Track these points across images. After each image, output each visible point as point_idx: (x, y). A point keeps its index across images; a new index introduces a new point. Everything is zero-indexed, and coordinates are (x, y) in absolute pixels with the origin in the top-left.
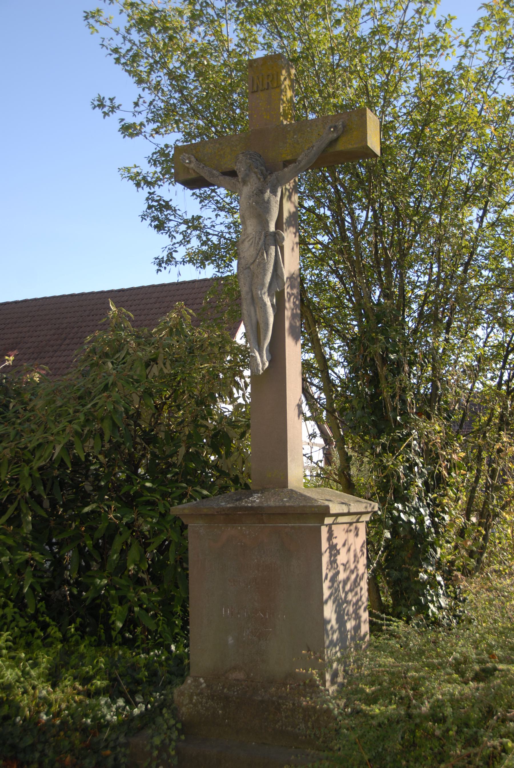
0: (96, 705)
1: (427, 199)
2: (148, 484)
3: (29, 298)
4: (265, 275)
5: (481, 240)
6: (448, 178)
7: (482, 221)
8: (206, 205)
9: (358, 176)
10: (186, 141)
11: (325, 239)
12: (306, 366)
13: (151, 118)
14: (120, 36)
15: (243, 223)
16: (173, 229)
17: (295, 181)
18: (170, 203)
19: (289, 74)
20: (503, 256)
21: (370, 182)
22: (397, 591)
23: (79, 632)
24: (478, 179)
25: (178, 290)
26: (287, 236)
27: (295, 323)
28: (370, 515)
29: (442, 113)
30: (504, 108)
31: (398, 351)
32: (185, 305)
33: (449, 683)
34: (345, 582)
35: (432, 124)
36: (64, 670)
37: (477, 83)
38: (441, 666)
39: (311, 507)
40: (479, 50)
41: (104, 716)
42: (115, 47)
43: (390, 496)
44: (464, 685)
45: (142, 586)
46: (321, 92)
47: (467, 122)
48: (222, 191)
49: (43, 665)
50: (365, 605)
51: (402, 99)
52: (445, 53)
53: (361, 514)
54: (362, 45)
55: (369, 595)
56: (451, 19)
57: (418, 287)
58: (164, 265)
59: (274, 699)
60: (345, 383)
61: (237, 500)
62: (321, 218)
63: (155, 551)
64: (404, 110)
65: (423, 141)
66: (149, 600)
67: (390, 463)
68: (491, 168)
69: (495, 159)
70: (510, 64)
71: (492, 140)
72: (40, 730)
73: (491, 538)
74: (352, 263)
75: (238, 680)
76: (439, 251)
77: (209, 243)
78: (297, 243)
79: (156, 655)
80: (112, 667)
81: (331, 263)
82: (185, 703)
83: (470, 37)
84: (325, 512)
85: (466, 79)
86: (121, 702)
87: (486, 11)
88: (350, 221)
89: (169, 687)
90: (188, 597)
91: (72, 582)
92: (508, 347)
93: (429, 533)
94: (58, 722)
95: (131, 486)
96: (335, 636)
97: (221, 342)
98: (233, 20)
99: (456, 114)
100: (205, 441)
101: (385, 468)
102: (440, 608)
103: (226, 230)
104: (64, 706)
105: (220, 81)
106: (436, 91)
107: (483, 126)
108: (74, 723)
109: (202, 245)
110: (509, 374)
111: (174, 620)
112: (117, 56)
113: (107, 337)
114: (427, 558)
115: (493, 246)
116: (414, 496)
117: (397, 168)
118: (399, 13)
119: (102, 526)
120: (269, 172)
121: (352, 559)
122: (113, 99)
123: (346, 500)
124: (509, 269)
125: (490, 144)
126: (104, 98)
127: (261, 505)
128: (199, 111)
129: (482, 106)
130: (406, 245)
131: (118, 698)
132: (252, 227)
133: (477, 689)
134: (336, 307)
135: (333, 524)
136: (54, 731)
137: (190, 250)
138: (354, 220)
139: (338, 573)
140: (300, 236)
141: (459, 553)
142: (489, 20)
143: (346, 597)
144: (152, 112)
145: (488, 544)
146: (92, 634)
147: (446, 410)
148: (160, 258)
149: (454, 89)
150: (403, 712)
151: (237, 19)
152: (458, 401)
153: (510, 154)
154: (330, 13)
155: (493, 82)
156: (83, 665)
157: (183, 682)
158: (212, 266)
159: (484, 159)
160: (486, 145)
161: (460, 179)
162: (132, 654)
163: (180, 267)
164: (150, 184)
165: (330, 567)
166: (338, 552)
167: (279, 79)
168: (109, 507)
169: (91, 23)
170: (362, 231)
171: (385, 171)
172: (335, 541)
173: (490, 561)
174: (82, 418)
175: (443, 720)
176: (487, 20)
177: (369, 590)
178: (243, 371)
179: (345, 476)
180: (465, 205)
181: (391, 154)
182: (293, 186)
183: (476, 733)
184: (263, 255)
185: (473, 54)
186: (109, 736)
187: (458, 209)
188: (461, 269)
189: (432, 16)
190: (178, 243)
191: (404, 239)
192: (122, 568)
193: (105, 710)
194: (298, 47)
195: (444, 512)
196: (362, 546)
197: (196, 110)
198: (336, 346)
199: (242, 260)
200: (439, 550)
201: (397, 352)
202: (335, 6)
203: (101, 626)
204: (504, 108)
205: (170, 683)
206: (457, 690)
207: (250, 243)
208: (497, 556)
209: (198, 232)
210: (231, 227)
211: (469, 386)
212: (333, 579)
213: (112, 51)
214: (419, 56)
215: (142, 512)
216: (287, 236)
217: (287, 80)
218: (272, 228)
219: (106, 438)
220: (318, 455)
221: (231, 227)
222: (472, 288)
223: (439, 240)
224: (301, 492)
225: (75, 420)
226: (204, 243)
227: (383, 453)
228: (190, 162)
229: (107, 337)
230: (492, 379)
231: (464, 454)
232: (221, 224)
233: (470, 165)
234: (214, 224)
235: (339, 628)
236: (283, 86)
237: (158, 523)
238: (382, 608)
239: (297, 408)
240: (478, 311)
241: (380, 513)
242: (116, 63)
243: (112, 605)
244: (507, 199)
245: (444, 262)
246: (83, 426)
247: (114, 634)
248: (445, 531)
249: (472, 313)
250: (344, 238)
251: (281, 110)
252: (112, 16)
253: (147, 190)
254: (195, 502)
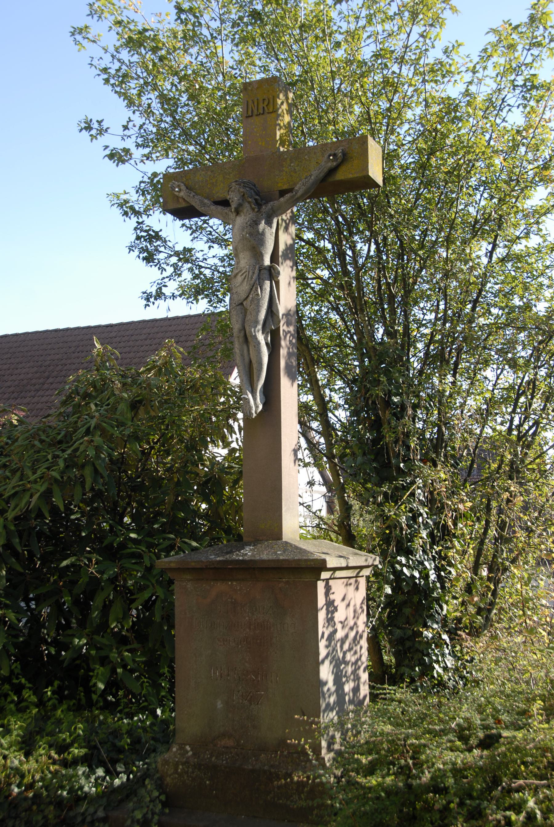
0: (73, 776)
1: (433, 232)
2: (133, 535)
3: (10, 333)
4: (258, 311)
5: (490, 276)
6: (455, 210)
7: (491, 257)
8: (197, 238)
9: (359, 207)
10: (179, 168)
11: (325, 274)
12: (304, 408)
13: (140, 143)
14: (108, 55)
15: (236, 255)
16: (163, 261)
17: (292, 212)
18: (160, 234)
19: (287, 98)
20: (513, 294)
21: (372, 213)
22: (400, 651)
23: (56, 696)
24: (487, 211)
25: (170, 326)
26: (284, 270)
27: (292, 363)
28: (371, 568)
29: (448, 142)
30: (514, 138)
31: (402, 393)
32: (177, 342)
33: (452, 750)
34: (343, 641)
35: (438, 153)
36: (38, 737)
37: (485, 111)
38: (443, 732)
39: (306, 560)
40: (487, 76)
41: (81, 788)
42: (104, 66)
43: (393, 548)
44: (467, 753)
45: (126, 645)
46: (320, 117)
47: (474, 151)
48: (215, 222)
49: (15, 733)
50: (364, 665)
51: (406, 127)
52: (453, 79)
53: (361, 568)
54: (364, 69)
55: (369, 654)
56: (459, 45)
57: (424, 325)
58: (152, 300)
59: (266, 768)
60: (345, 427)
61: (227, 553)
62: (321, 251)
63: (140, 607)
64: (409, 139)
65: (429, 171)
66: (134, 661)
67: (392, 513)
68: (500, 200)
69: (504, 191)
70: (519, 91)
71: (502, 170)
72: (10, 804)
73: (501, 593)
74: (353, 299)
75: (227, 747)
76: (446, 288)
77: (202, 276)
78: (294, 278)
79: (140, 720)
80: (91, 734)
81: (332, 299)
82: (169, 773)
83: (478, 63)
84: (321, 566)
85: (473, 107)
86: (100, 772)
87: (494, 36)
88: (351, 255)
89: (153, 755)
90: (174, 658)
91: (49, 640)
92: (519, 389)
93: (435, 588)
94: (31, 795)
95: (115, 537)
96: (332, 700)
97: (213, 382)
98: (229, 41)
99: (463, 142)
100: (195, 488)
101: (388, 518)
102: (445, 669)
103: (220, 264)
104: (37, 777)
105: (214, 105)
106: (442, 118)
107: (492, 156)
108: (48, 796)
109: (194, 278)
110: (520, 418)
111: (160, 681)
112: (106, 76)
113: (91, 376)
114: (432, 615)
115: (503, 282)
116: (417, 549)
117: (401, 199)
118: (403, 36)
119: (83, 580)
120: (264, 202)
121: (352, 615)
122: (102, 121)
123: (344, 554)
124: (519, 307)
125: (499, 176)
126: (91, 120)
127: (253, 558)
128: (191, 136)
129: (491, 135)
130: (411, 280)
131: (97, 768)
132: (245, 261)
133: (481, 757)
134: (336, 346)
135: (330, 578)
136: (25, 805)
137: (183, 283)
138: (356, 255)
139: (335, 631)
140: (297, 270)
141: (466, 610)
142: (496, 46)
143: (344, 657)
144: (142, 137)
145: (497, 600)
146: (70, 697)
147: (453, 456)
148: (148, 292)
149: (461, 116)
150: (401, 784)
151: (233, 40)
152: (467, 447)
153: (519, 186)
154: (330, 35)
155: (502, 111)
156: (60, 732)
157: (168, 749)
158: (206, 300)
159: (493, 190)
160: (496, 176)
161: (468, 211)
162: (114, 719)
163: (169, 301)
164: (137, 213)
165: (327, 624)
166: (336, 609)
167: (275, 103)
168: (90, 560)
169: (77, 39)
170: (363, 265)
171: (389, 202)
172: (332, 597)
173: (500, 619)
174: (62, 464)
175: (444, 791)
176: (495, 46)
177: (369, 650)
178: (237, 414)
179: (345, 526)
180: (473, 238)
181: (394, 184)
182: (291, 217)
183: (479, 805)
184: (257, 290)
185: (480, 81)
186: (86, 810)
187: (465, 244)
188: (469, 306)
189: (437, 40)
190: (167, 277)
191: (408, 274)
192: (104, 626)
193: (83, 781)
194: (297, 70)
195: (450, 564)
196: (362, 603)
197: (189, 135)
198: (337, 387)
199: (235, 296)
200: (445, 606)
201: (400, 395)
202: (335, 28)
203: (81, 689)
204: (514, 138)
205: (154, 751)
206: (459, 758)
207: (243, 277)
208: (506, 612)
209: (190, 265)
210: (225, 260)
211: (478, 431)
212: (331, 637)
213: (101, 71)
214: (424, 81)
215: (124, 565)
216: (284, 270)
217: (285, 104)
218: (267, 262)
219: (88, 487)
220: (320, 505)
221: (225, 260)
222: (480, 327)
223: (446, 275)
224: (297, 544)
225: (54, 466)
226: (196, 277)
227: (384, 502)
228: (180, 190)
229: (91, 376)
230: (502, 424)
231: (471, 504)
232: (214, 257)
233: (478, 196)
234: (205, 257)
235: (337, 691)
236: (280, 111)
237: (142, 577)
238: (385, 669)
239: (293, 453)
240: (487, 351)
241: (380, 567)
242: (104, 84)
243: (92, 666)
244: (517, 233)
245: (451, 300)
246: (62, 473)
247: (94, 697)
248: (451, 586)
249: (481, 353)
250: (346, 273)
251: (278, 138)
252: (101, 34)
253: (134, 219)
254: (182, 555)
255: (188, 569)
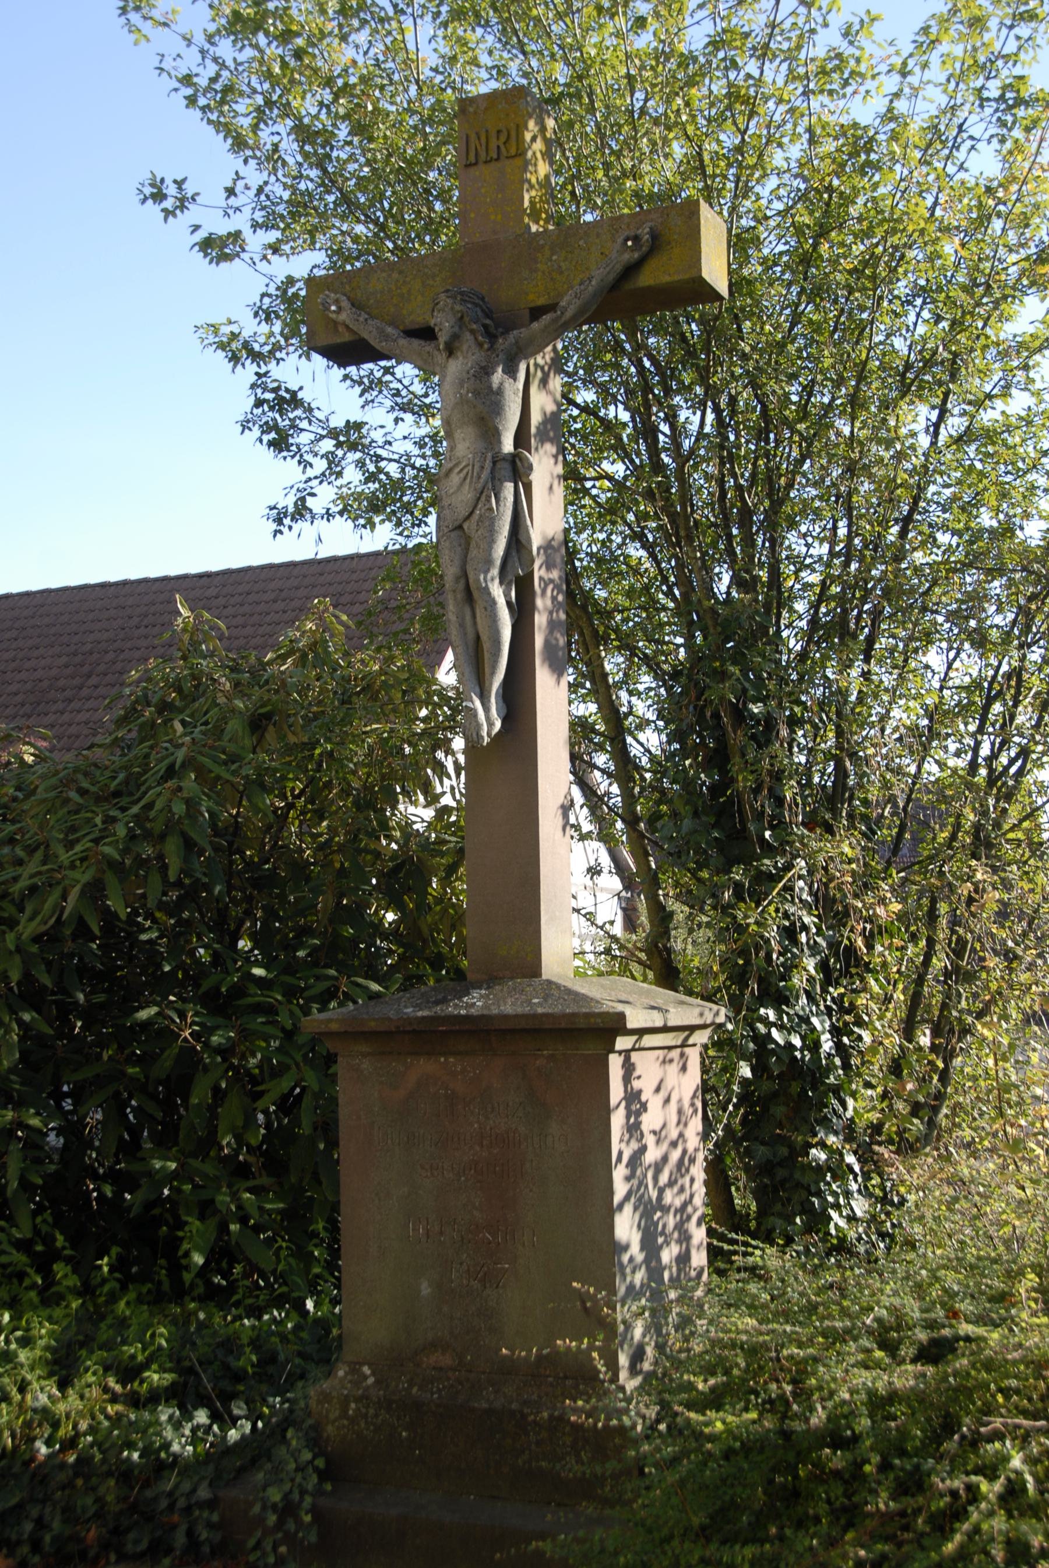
75: (441, 1369)
255: (363, 1033)
